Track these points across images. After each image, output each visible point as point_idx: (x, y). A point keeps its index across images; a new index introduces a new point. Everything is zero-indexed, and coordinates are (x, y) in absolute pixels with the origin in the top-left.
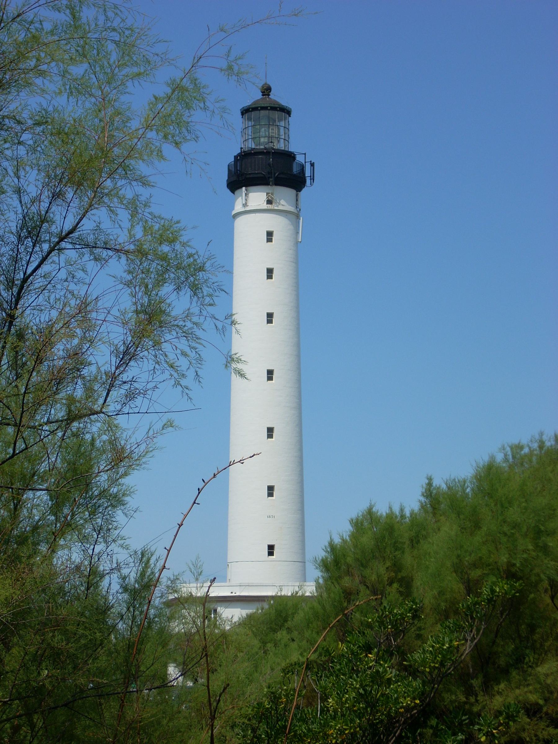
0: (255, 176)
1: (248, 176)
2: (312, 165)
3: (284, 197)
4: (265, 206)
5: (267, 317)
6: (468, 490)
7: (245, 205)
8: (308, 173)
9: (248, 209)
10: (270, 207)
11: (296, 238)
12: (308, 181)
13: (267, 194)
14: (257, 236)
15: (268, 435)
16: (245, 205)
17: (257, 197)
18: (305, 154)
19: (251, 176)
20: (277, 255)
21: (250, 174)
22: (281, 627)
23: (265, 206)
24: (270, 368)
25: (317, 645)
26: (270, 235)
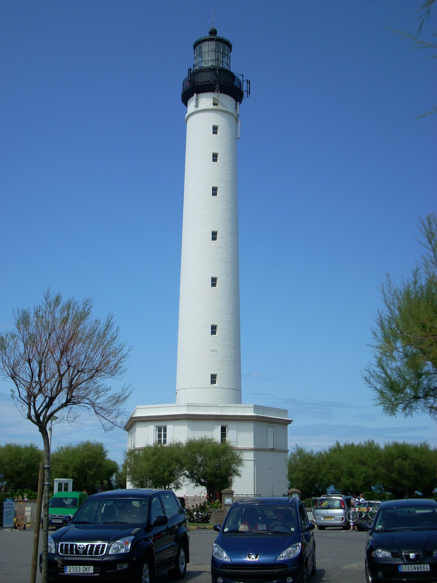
0: (205, 83)
1: (199, 84)
2: (248, 82)
3: (227, 101)
4: (212, 107)
5: (212, 281)
6: (424, 292)
7: (197, 106)
8: (245, 88)
9: (198, 109)
10: (216, 107)
11: (236, 135)
12: (245, 94)
13: (213, 98)
14: (204, 125)
15: (213, 193)
16: (197, 106)
17: (206, 100)
18: (243, 75)
19: (202, 84)
20: (220, 144)
21: (200, 82)
22: (345, 493)
23: (212, 107)
24: (215, 230)
25: (395, 528)
26: (215, 130)
